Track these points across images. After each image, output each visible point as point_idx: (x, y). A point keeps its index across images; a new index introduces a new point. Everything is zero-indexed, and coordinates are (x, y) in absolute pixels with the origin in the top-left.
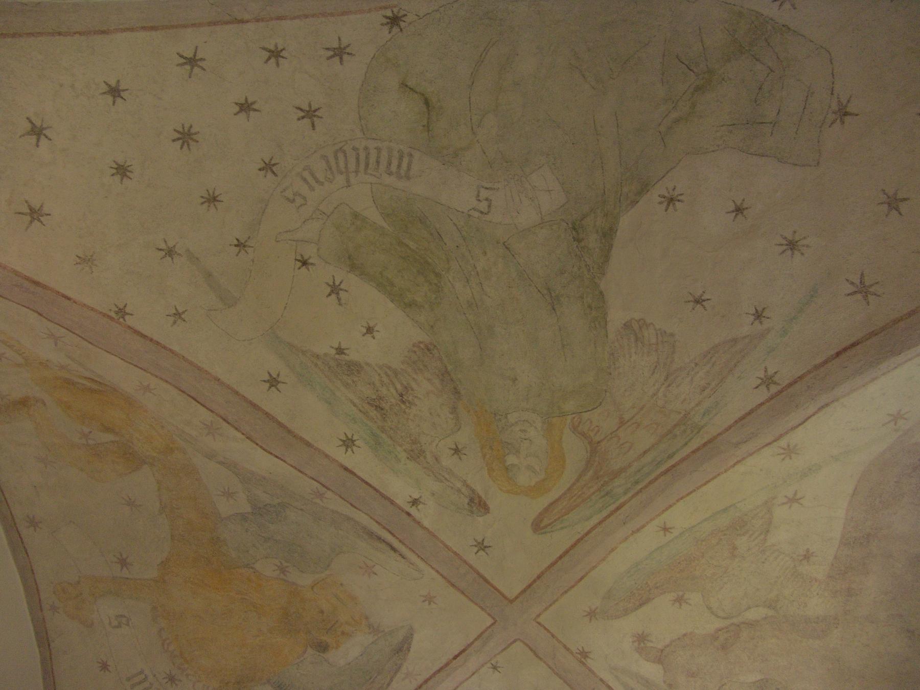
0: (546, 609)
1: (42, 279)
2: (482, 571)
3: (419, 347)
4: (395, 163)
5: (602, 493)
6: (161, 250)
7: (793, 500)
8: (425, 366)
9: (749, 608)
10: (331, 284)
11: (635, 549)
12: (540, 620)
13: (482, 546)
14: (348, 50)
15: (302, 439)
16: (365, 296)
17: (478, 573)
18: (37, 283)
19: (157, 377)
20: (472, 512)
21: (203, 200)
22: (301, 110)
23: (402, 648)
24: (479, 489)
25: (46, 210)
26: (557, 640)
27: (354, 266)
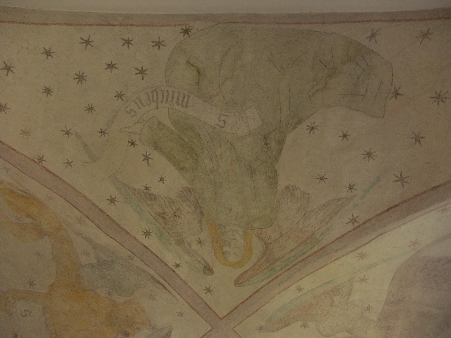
0: (238, 324)
2: (208, 303)
4: (181, 99)
5: (269, 269)
6: (63, 131)
7: (363, 280)
9: (338, 332)
10: (145, 155)
11: (284, 298)
12: (235, 329)
13: (209, 290)
14: (163, 43)
15: (124, 230)
16: (160, 162)
17: (206, 304)
20: (205, 273)
21: (86, 109)
24: (210, 262)
25: (8, 106)
27: (156, 147)
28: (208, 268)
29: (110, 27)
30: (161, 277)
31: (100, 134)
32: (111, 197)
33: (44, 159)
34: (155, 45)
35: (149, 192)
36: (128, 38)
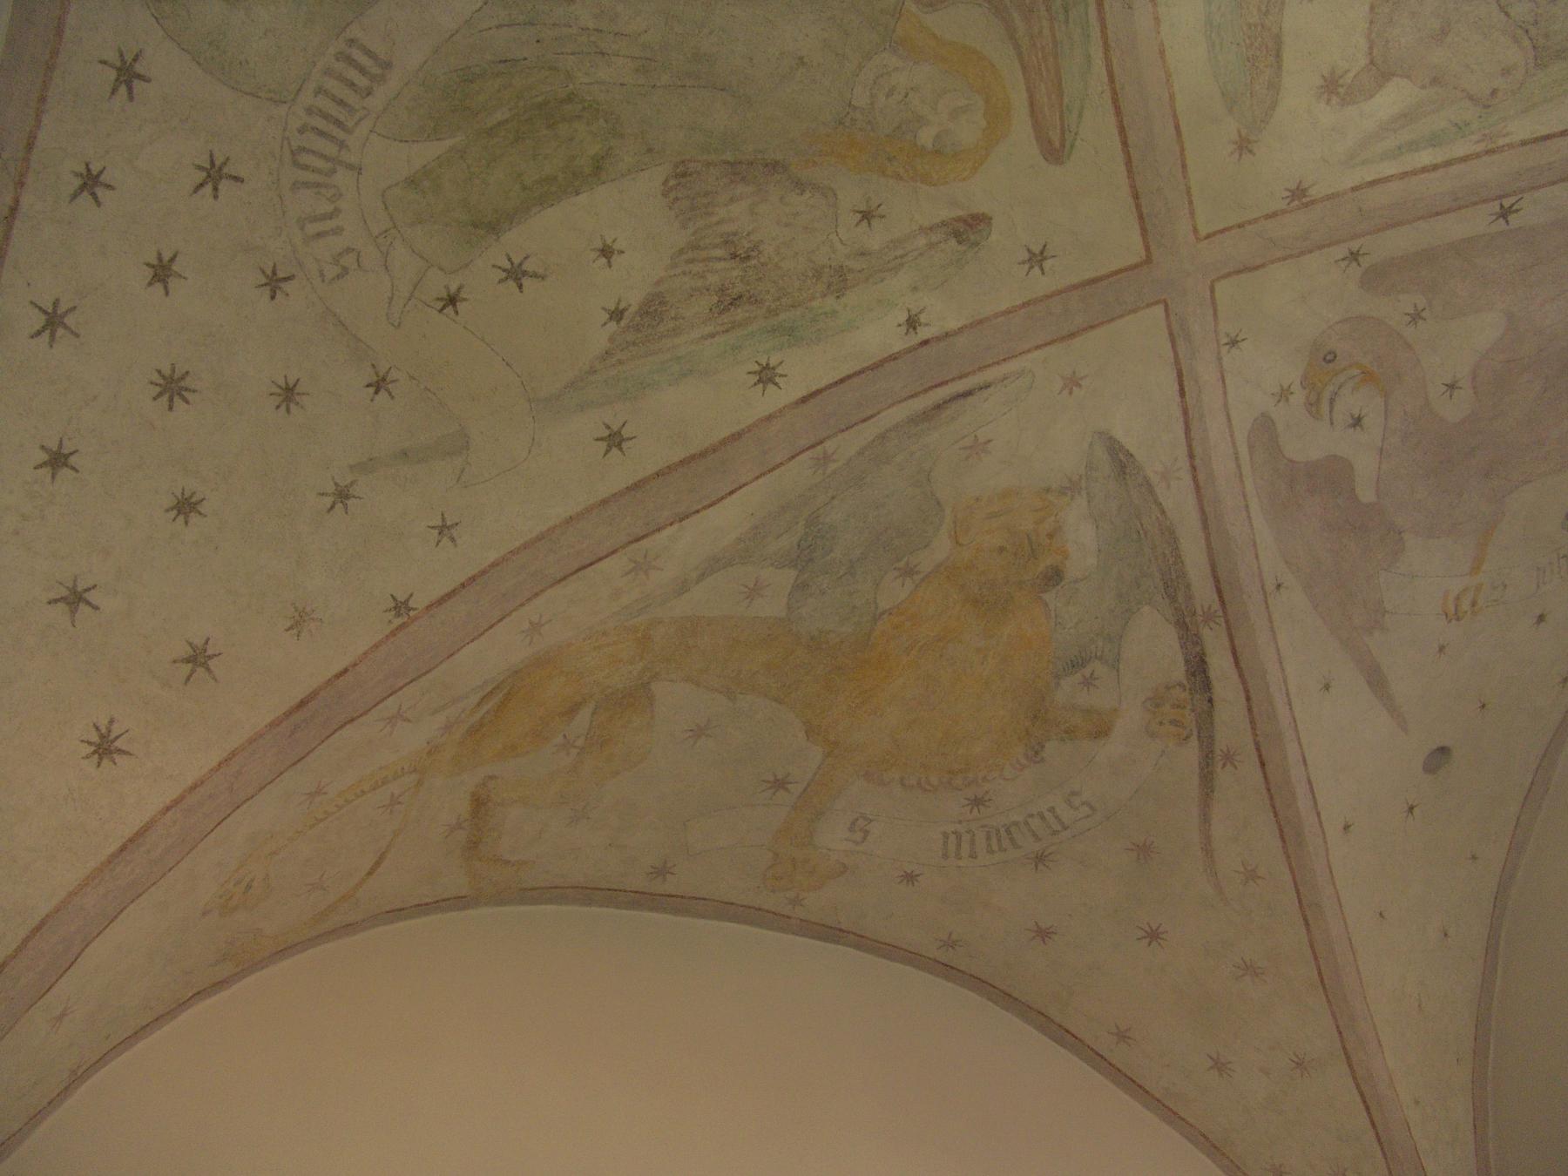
0: (1192, 213)
1: (299, 694)
2: (1075, 280)
3: (671, 189)
4: (353, 74)
5: (1061, 17)
6: (332, 507)
8: (706, 194)
10: (504, 275)
12: (1203, 231)
13: (1037, 259)
14: (129, 58)
15: (724, 442)
16: (547, 233)
17: (1075, 287)
18: (302, 704)
19: (522, 605)
21: (283, 407)
22: (202, 185)
23: (1122, 462)
24: (946, 214)
26: (1250, 222)
28: (961, 227)
29: (17, 223)
30: (926, 391)
31: (383, 393)
32: (601, 439)
33: (401, 598)
34: (130, 89)
35: (632, 309)
36: (77, 175)
